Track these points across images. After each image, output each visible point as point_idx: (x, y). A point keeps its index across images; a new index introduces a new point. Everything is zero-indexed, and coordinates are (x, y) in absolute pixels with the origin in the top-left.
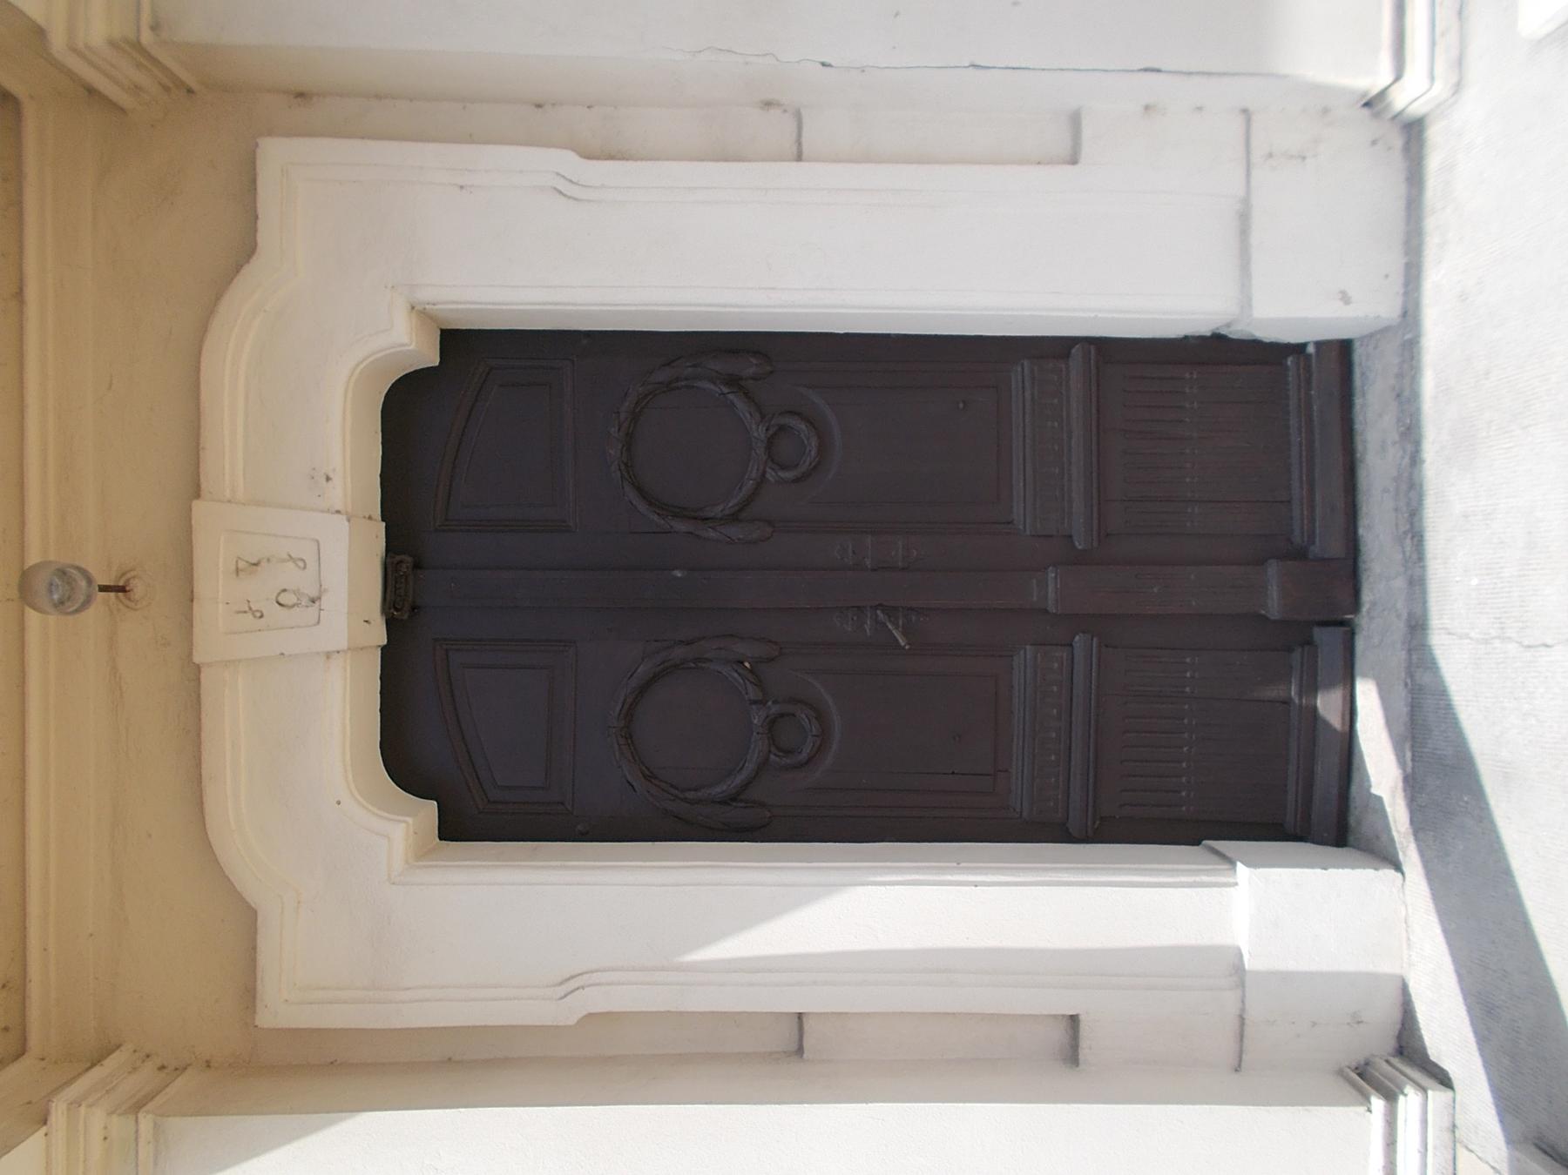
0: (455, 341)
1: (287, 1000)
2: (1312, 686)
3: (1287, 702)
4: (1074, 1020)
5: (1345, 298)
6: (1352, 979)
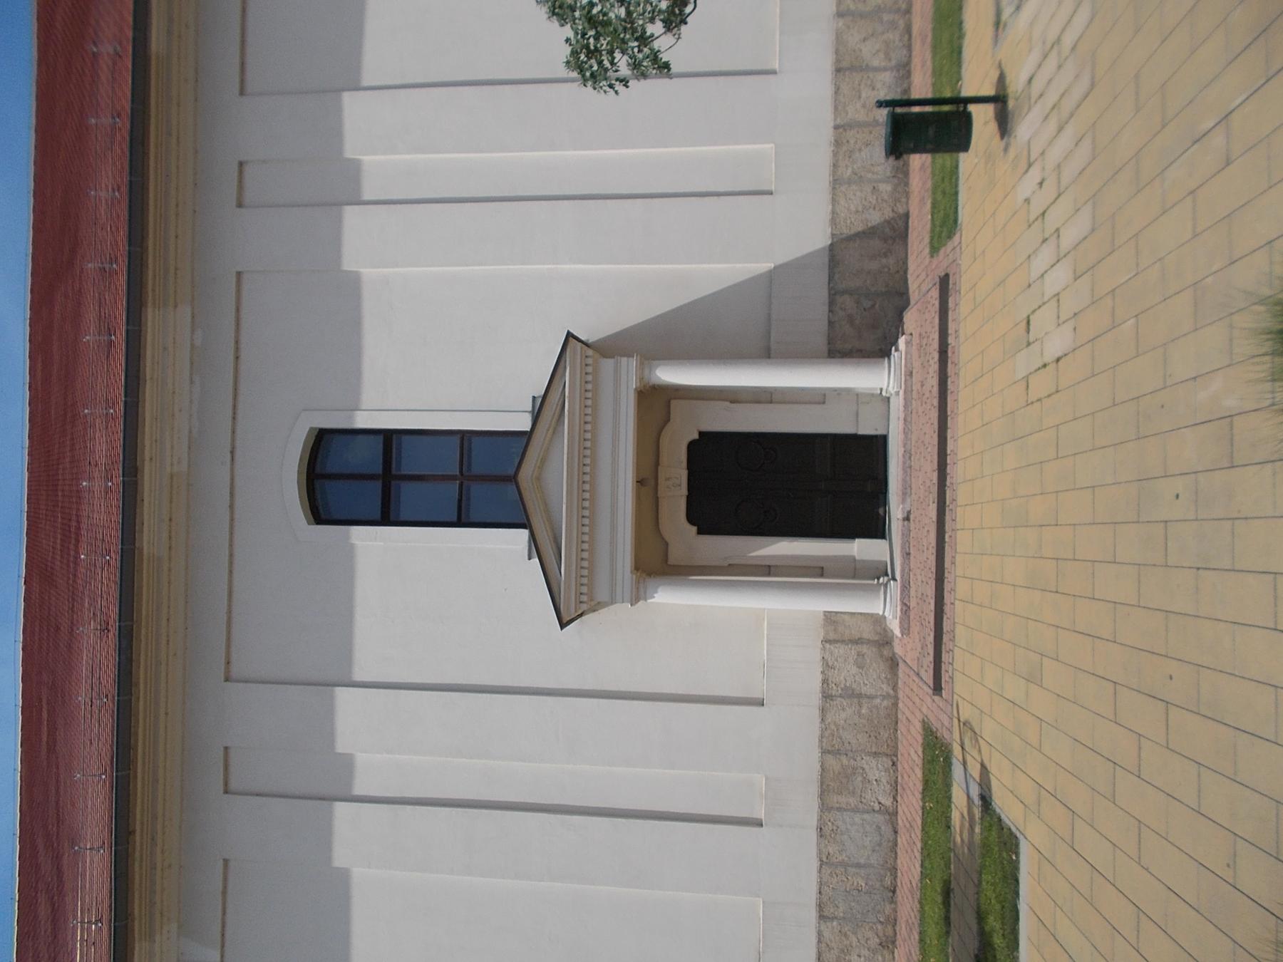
0: (701, 433)
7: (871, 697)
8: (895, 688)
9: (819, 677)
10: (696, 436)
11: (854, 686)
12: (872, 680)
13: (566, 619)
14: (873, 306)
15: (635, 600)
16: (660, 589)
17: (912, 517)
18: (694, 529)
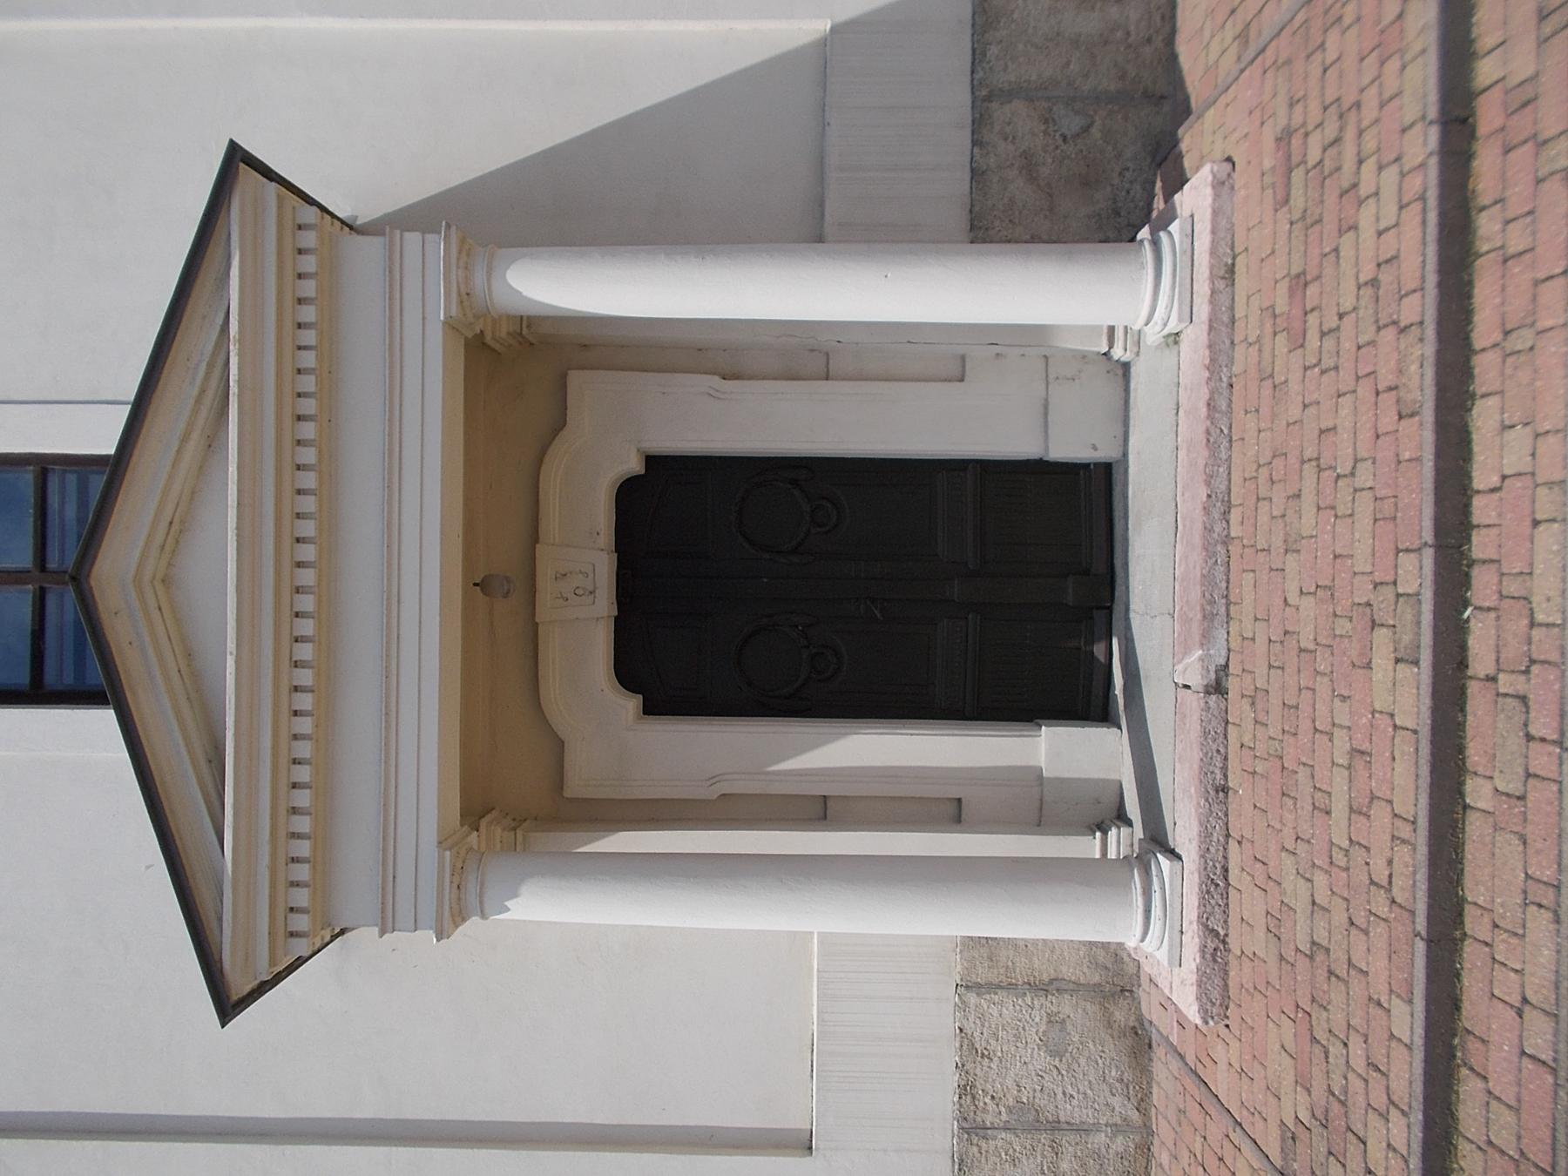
0: (652, 461)
1: (576, 786)
2: (1091, 642)
3: (1079, 649)
4: (959, 800)
5: (1095, 448)
6: (1097, 781)
7: (1082, 1129)
8: (1143, 1104)
9: (953, 1079)
10: (635, 466)
11: (1041, 1101)
12: (1088, 1089)
13: (239, 985)
14: (1086, 129)
15: (453, 913)
16: (525, 889)
17: (1232, 684)
18: (633, 703)
